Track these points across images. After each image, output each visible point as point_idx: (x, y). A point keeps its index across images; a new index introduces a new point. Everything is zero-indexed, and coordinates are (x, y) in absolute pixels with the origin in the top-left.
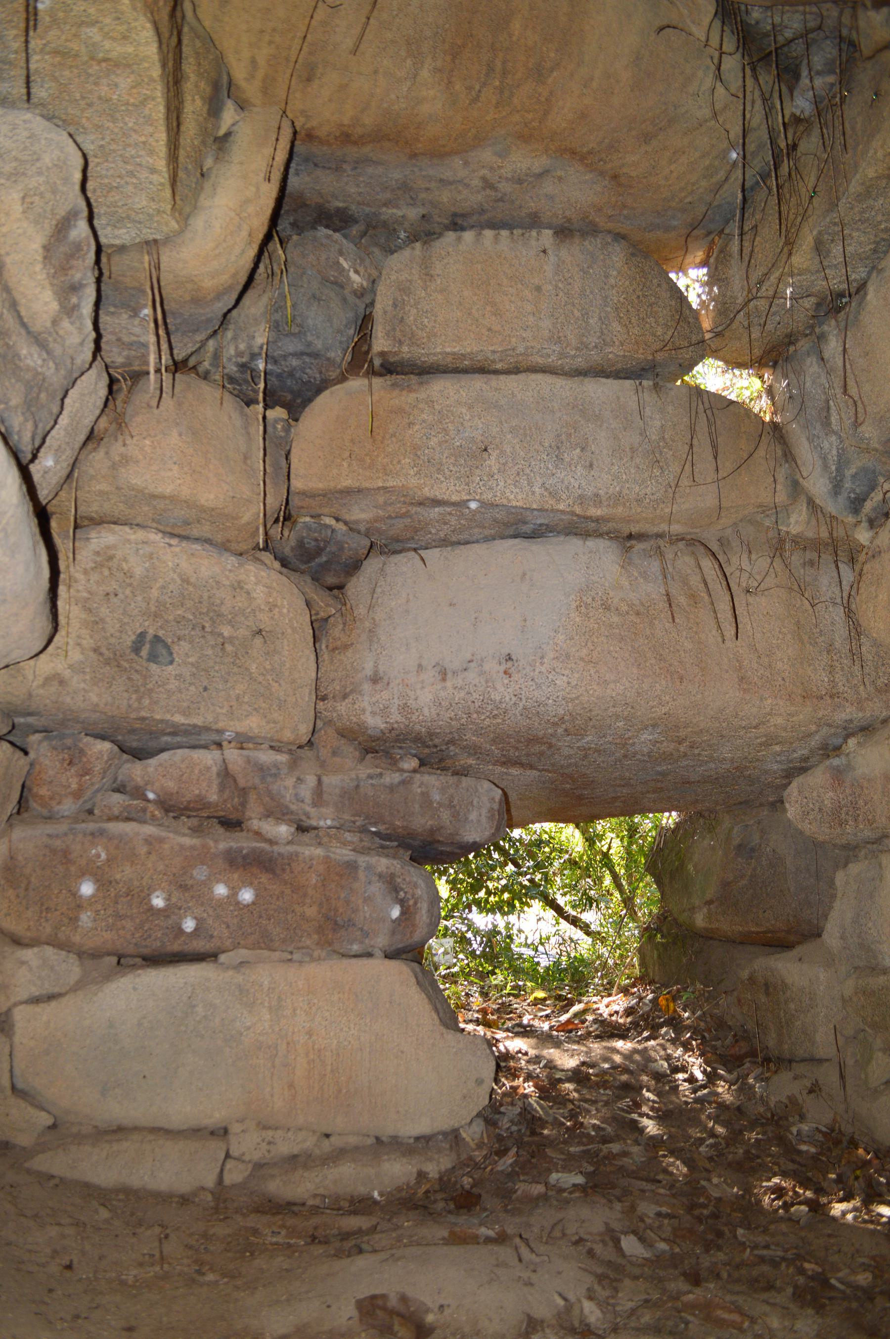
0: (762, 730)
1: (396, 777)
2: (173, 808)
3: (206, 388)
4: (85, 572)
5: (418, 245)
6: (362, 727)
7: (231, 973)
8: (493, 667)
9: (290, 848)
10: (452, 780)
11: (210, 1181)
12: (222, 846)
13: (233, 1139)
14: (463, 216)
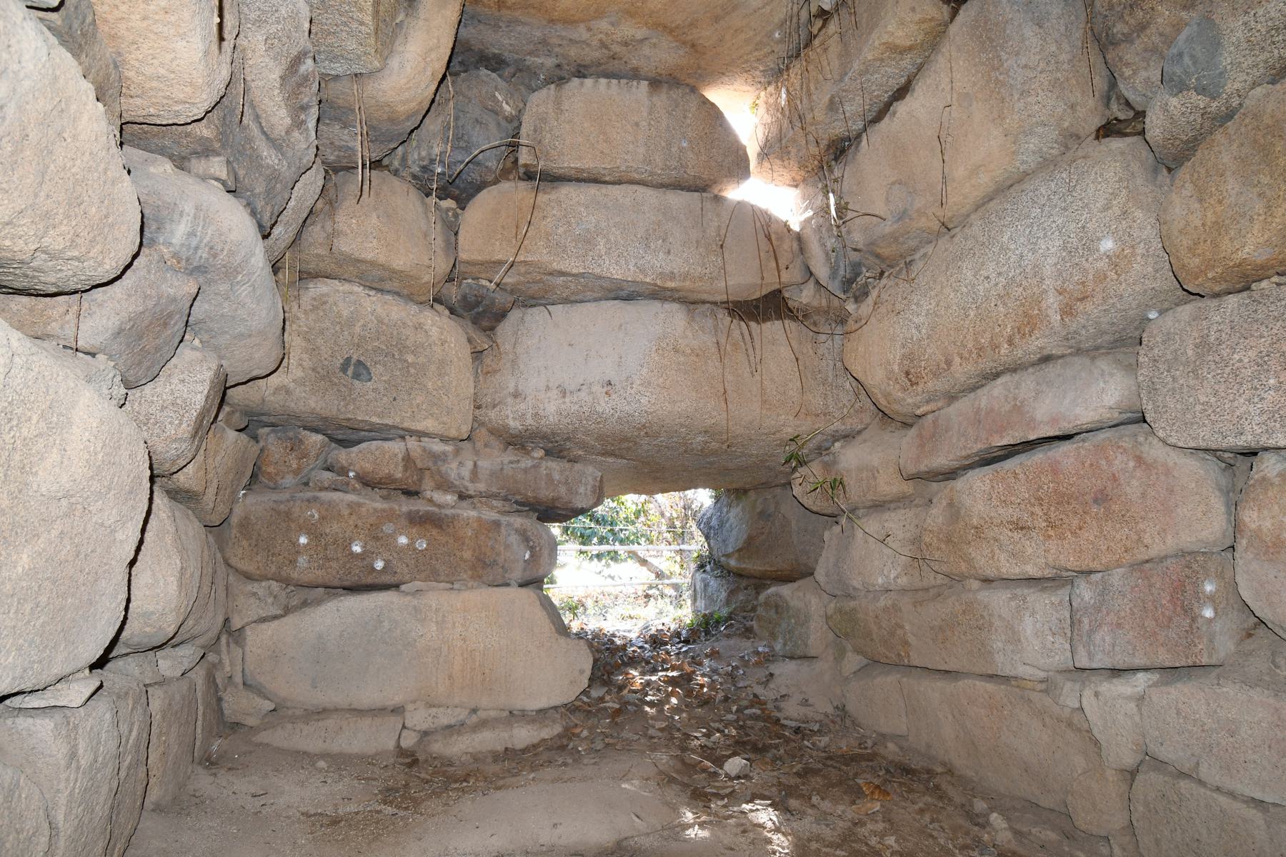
0: (778, 435)
1: (529, 463)
2: (368, 482)
3: (396, 182)
4: (306, 312)
5: (553, 86)
6: (506, 428)
7: (409, 598)
8: (597, 389)
9: (452, 511)
10: (568, 465)
11: (391, 745)
12: (405, 509)
13: (407, 715)
14: (585, 66)
